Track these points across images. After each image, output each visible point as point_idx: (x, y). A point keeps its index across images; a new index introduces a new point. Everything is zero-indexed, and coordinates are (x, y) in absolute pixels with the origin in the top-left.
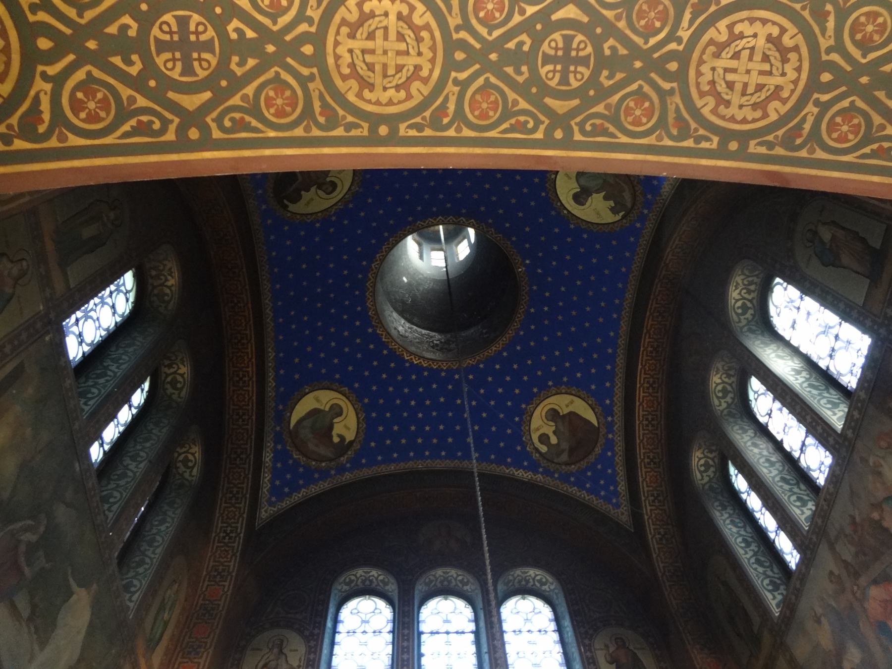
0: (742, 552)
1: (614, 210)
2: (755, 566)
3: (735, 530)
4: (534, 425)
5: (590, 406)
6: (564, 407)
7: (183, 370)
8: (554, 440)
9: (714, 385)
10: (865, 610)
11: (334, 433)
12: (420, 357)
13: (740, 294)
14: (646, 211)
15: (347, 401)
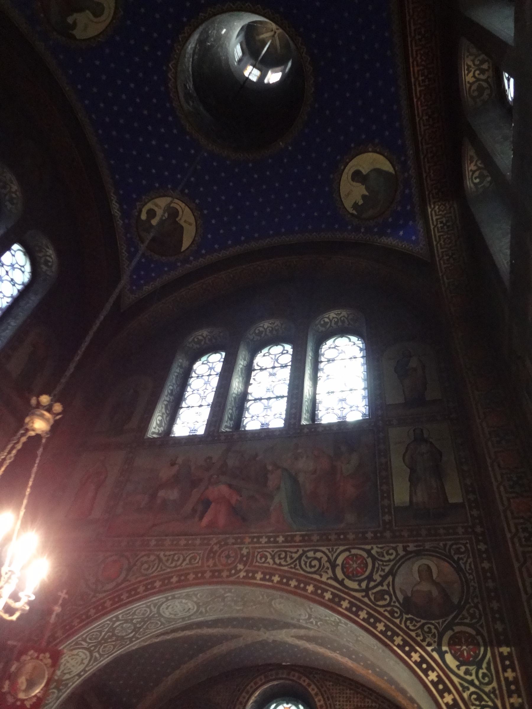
0: (166, 393)
1: (355, 205)
2: (164, 406)
3: (174, 381)
4: (157, 201)
5: (194, 240)
6: (183, 220)
7: (469, 78)
8: (154, 222)
9: (262, 325)
10: (207, 488)
11: (76, 16)
12: (175, 78)
13: (333, 318)
14: (363, 230)
15: (110, 19)
